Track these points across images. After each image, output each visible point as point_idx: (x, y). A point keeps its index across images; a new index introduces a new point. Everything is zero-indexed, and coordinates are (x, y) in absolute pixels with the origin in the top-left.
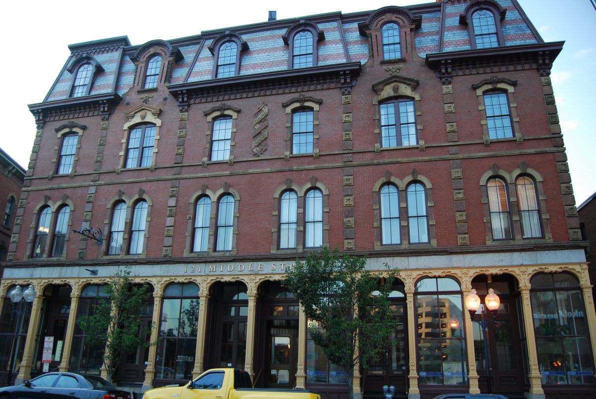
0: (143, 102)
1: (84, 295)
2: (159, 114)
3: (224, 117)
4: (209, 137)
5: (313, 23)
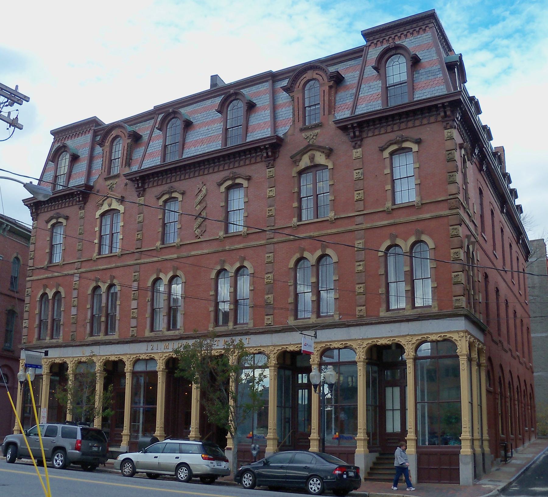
0: (109, 188)
1: (78, 372)
2: (122, 200)
3: (402, 150)
4: (389, 176)
5: (323, 66)
